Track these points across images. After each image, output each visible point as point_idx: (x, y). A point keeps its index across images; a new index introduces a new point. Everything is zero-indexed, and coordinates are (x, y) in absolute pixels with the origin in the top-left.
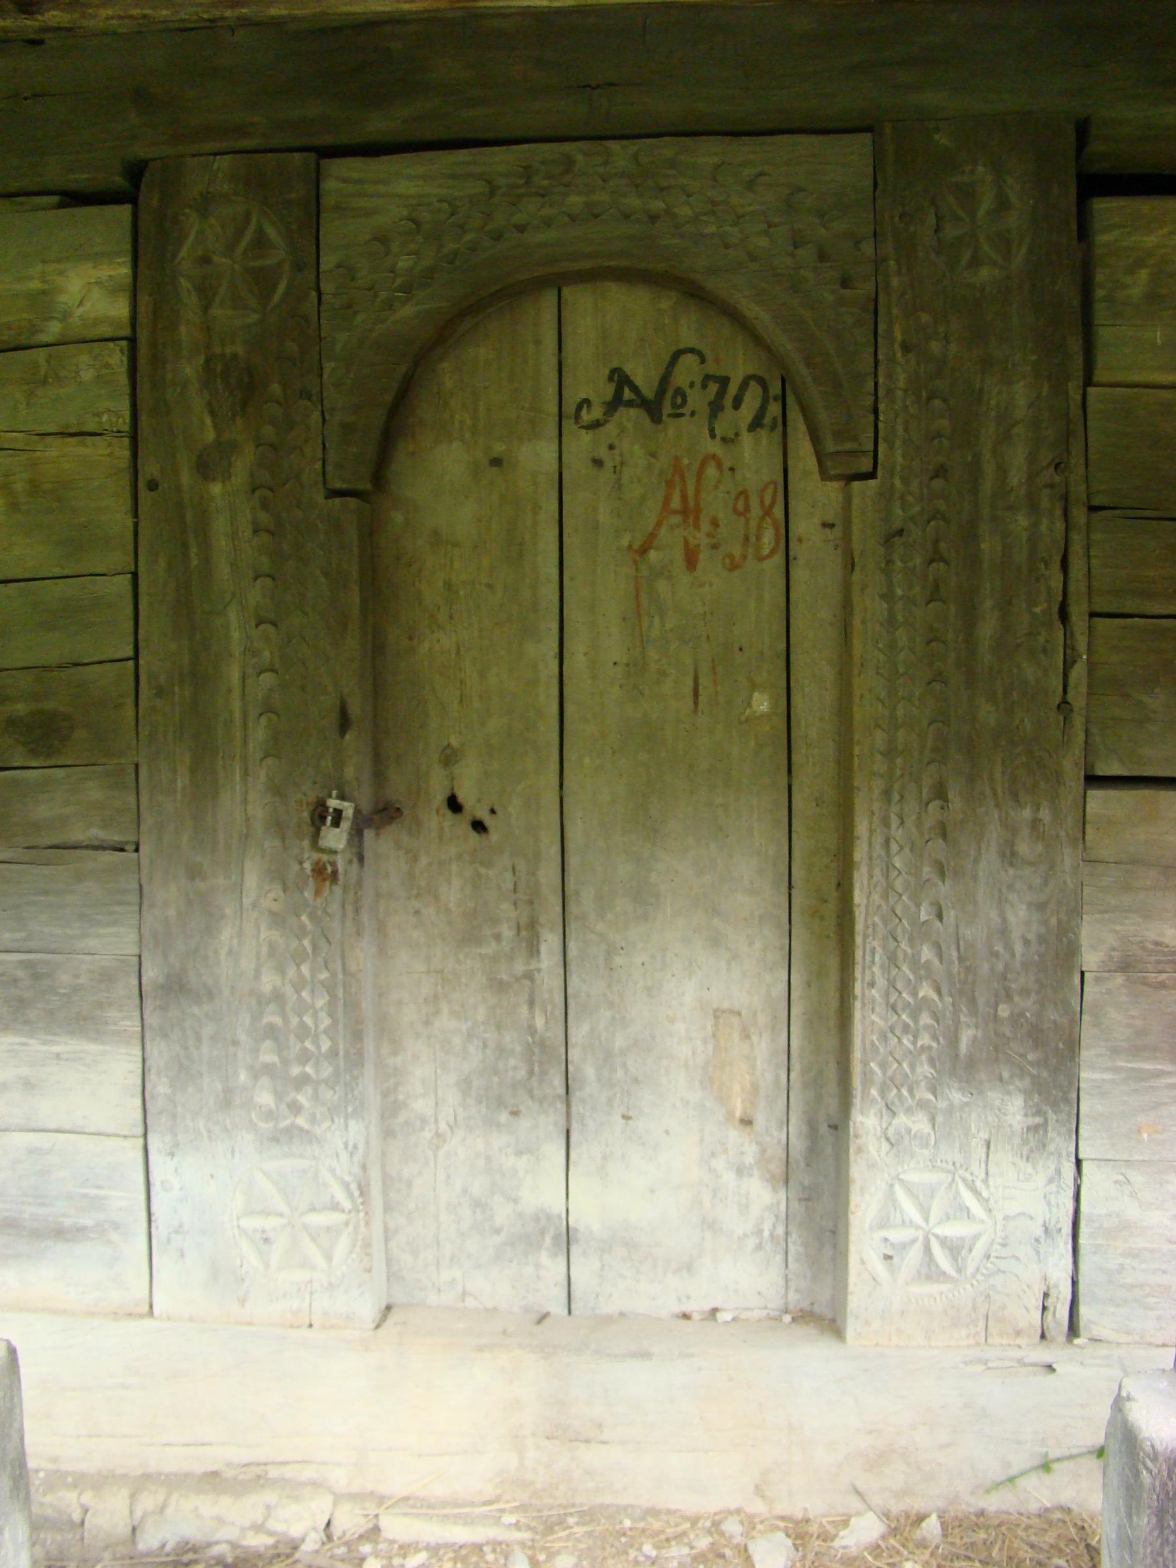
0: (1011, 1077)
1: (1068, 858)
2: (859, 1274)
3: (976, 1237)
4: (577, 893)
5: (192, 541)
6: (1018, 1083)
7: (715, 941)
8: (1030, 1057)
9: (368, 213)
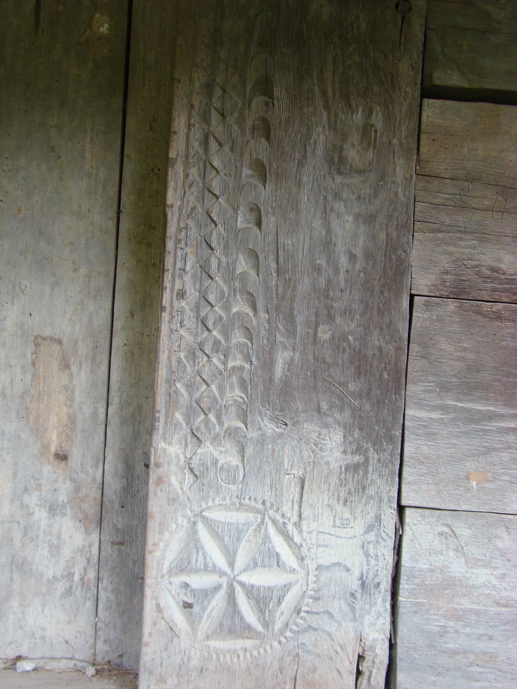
0: (331, 408)
1: (400, 169)
2: (155, 624)
3: (286, 588)
6: (337, 416)
8: (352, 387)
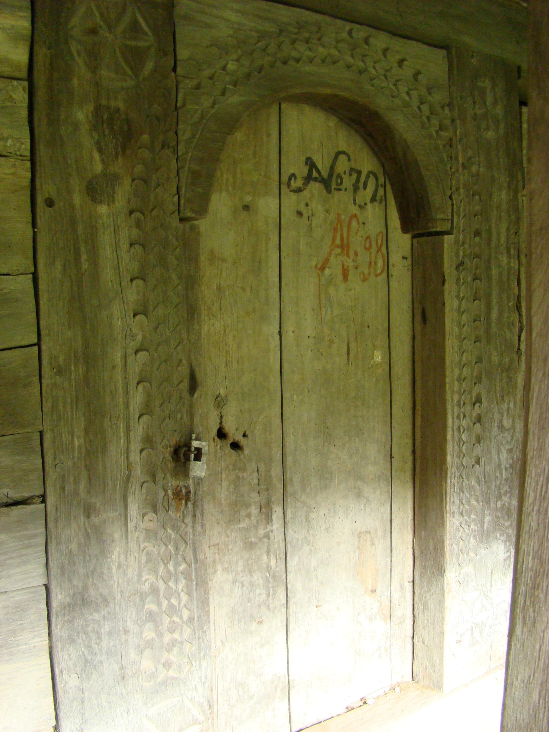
4: (291, 479)
5: (83, 249)
6: (502, 538)
7: (359, 495)
9: (209, 26)
